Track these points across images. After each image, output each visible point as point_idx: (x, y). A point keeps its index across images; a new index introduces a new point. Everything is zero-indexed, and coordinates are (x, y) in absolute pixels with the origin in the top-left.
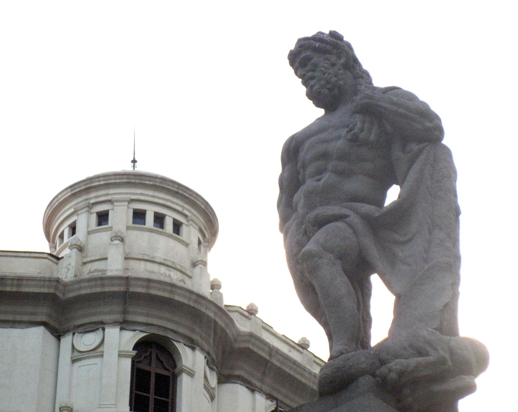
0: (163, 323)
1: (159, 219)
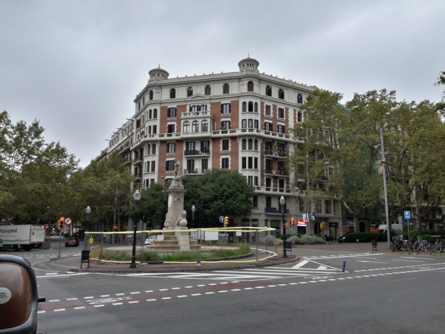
0: (251, 79)
1: (250, 64)
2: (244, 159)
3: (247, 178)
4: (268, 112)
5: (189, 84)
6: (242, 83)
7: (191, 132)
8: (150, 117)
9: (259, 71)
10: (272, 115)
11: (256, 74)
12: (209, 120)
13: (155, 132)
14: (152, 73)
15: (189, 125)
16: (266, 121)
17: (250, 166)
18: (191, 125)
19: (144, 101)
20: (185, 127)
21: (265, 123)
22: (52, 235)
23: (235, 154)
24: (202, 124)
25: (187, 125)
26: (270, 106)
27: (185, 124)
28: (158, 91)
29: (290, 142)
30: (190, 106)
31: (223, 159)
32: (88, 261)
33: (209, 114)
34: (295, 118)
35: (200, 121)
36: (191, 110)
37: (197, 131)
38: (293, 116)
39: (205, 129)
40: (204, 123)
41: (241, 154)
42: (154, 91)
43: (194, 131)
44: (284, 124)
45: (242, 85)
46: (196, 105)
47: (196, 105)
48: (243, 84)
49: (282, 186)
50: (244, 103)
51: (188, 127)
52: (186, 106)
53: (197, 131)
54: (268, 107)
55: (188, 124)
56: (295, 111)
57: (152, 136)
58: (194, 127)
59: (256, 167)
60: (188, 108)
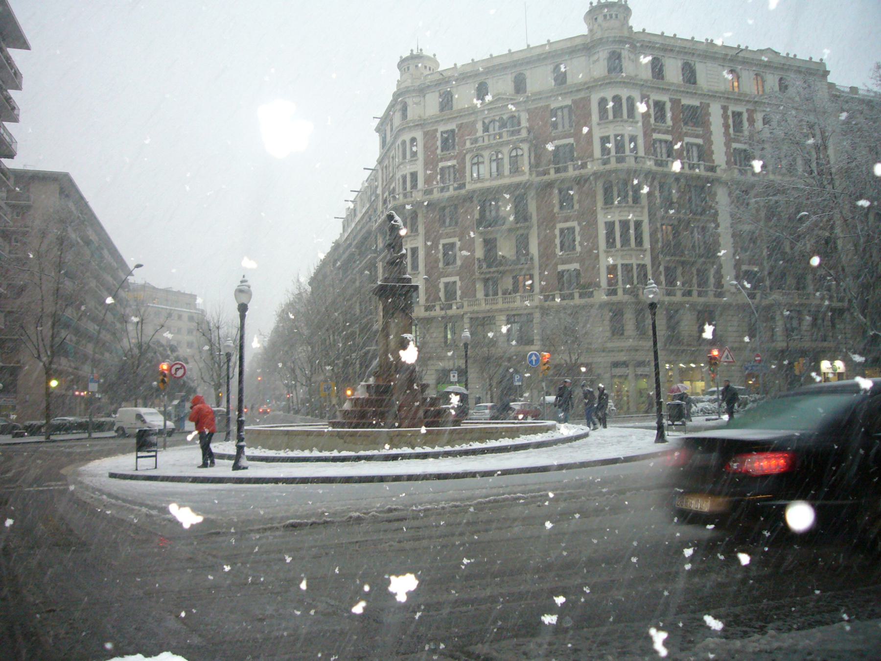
0: (616, 47)
2: (610, 226)
3: (635, 267)
4: (738, 126)
5: (465, 75)
6: (596, 57)
7: (488, 176)
8: (404, 157)
9: (631, 27)
10: (669, 122)
11: (626, 34)
12: (525, 146)
13: (414, 186)
14: (404, 64)
15: (483, 163)
16: (655, 136)
17: (625, 241)
18: (487, 161)
19: (392, 125)
20: (475, 168)
21: (655, 141)
22: (452, 383)
23: (588, 218)
24: (510, 157)
25: (478, 163)
26: (664, 103)
27: (475, 160)
28: (416, 100)
29: (717, 180)
30: (484, 123)
31: (562, 231)
32: (153, 454)
33: (524, 134)
34: (726, 126)
35: (506, 150)
36: (486, 129)
37: (500, 174)
38: (722, 121)
39: (515, 170)
40: (514, 154)
41: (603, 218)
42: (410, 101)
43: (495, 174)
44: (700, 141)
45: (595, 62)
46: (497, 118)
47: (497, 118)
48: (598, 60)
49: (703, 283)
50: (603, 102)
51: (481, 166)
52: (474, 123)
53: (500, 174)
54: (737, 115)
55: (481, 160)
56: (725, 108)
57: (409, 194)
58: (494, 165)
59: (639, 241)
60: (479, 126)
